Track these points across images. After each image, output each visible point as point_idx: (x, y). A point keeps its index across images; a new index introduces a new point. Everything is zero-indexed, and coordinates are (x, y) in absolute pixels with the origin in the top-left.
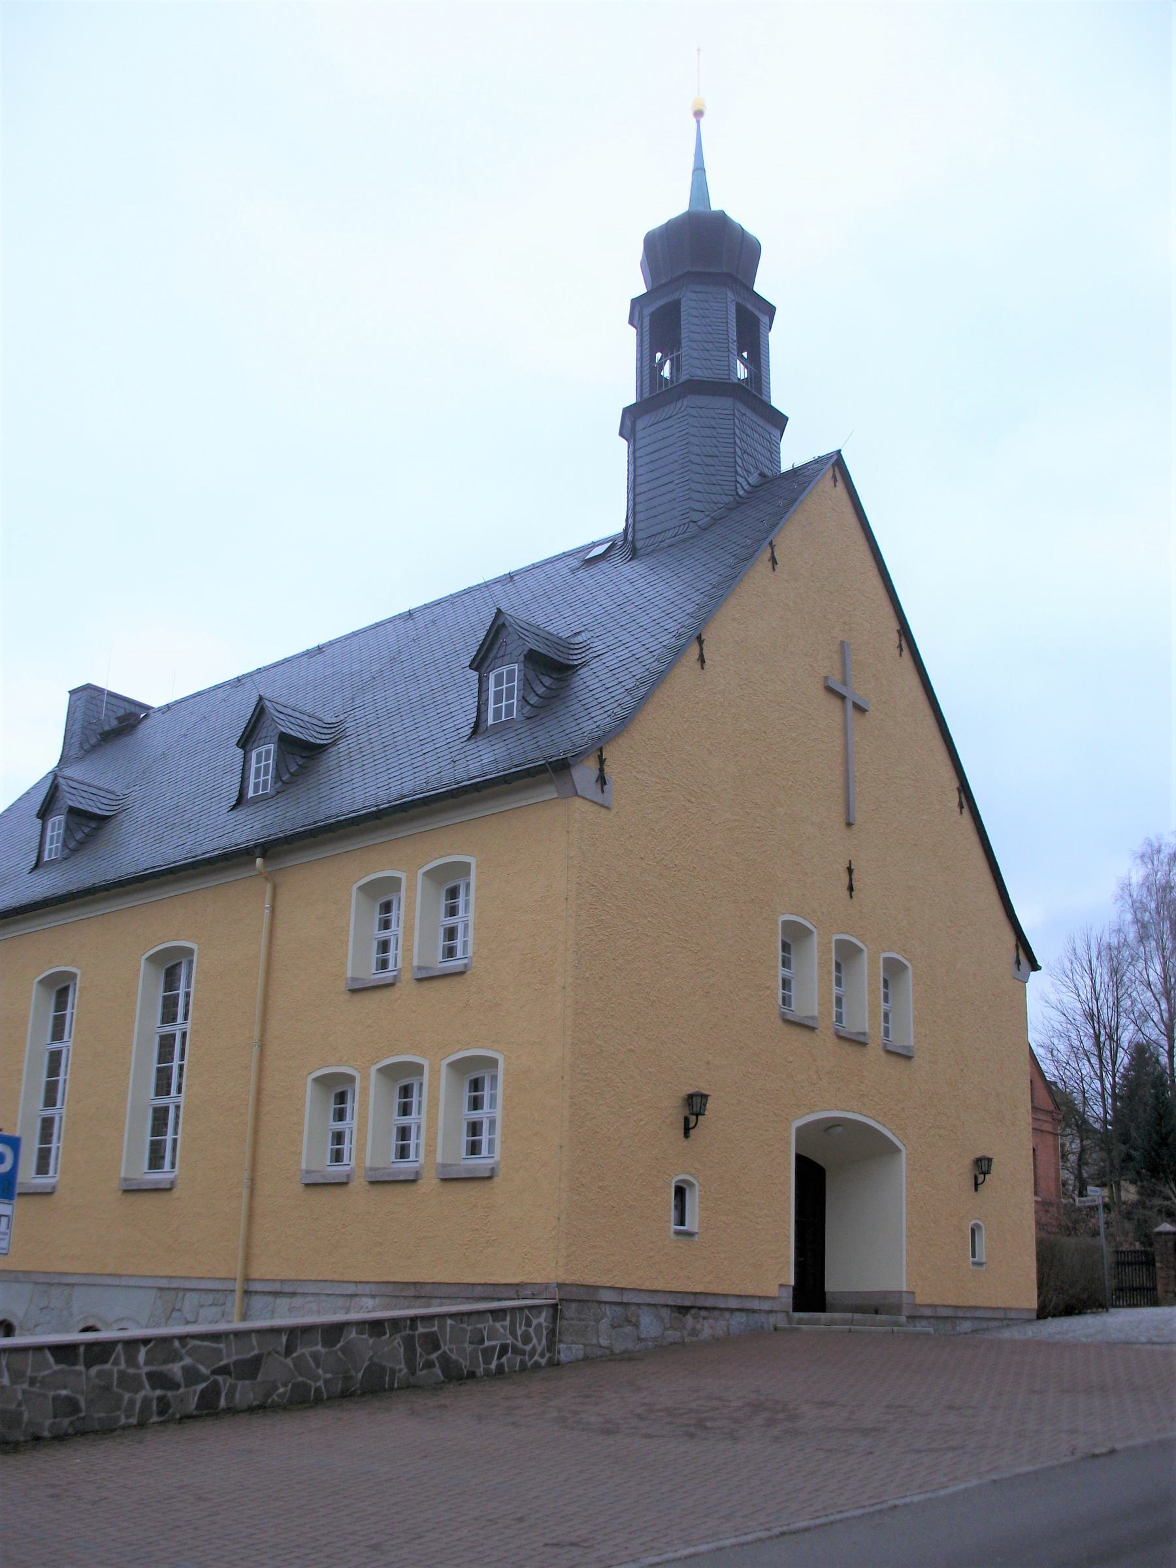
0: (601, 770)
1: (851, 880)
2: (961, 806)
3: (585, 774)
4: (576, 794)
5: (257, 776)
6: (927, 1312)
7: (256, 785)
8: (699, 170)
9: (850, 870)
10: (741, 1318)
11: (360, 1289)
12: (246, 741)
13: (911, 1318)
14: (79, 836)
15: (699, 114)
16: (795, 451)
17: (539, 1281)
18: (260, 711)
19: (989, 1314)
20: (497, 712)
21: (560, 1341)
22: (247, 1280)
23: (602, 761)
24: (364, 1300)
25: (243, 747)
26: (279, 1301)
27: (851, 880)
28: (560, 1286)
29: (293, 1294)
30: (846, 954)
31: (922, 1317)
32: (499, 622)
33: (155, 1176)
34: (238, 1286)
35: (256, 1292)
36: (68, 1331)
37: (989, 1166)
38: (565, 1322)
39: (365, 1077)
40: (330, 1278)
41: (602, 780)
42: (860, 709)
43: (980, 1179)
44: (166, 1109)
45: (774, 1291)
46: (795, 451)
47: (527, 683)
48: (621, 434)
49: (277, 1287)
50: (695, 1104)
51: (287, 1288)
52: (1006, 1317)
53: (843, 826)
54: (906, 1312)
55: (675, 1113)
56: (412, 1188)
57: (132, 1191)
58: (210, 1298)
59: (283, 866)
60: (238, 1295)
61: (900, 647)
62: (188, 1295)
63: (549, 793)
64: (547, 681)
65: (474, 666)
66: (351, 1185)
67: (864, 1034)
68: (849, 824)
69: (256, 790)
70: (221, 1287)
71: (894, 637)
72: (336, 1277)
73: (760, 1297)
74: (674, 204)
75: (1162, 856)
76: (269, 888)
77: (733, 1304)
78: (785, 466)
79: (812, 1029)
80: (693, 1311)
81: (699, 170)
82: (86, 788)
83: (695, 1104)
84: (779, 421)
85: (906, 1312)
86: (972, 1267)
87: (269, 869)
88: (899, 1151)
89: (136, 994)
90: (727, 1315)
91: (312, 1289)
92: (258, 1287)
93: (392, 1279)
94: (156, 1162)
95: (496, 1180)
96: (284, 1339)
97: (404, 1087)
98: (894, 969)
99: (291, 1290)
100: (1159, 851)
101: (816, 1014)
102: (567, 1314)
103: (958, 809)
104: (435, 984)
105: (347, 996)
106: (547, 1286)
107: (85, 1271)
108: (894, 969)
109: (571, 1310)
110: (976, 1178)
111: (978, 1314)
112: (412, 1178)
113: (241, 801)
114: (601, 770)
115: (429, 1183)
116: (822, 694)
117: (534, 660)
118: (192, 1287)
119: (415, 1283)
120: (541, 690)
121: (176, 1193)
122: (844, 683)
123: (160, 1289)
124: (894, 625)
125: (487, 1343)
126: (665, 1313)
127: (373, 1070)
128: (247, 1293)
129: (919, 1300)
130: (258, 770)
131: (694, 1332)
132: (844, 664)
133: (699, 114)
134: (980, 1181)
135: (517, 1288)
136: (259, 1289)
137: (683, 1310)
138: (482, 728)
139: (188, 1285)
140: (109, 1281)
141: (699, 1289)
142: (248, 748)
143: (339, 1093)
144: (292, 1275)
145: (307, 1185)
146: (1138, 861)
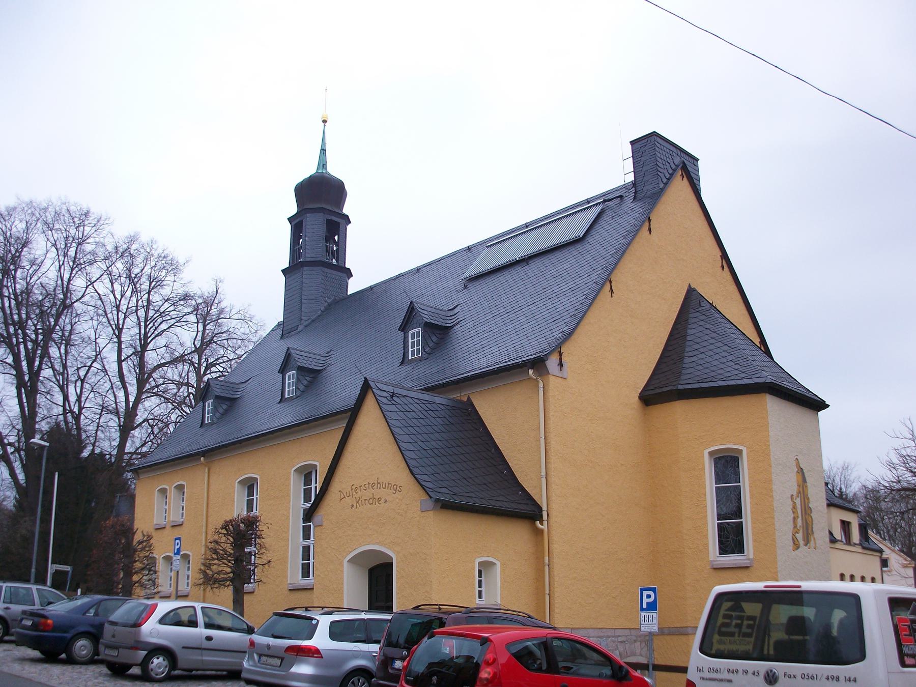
0: (561, 359)
5: (413, 347)
7: (413, 352)
8: (323, 150)
12: (283, 370)
14: (221, 411)
15: (325, 121)
18: (411, 309)
23: (561, 354)
36: (828, 579)
41: (561, 365)
44: (309, 547)
47: (298, 380)
48: (654, 134)
64: (308, 379)
69: (413, 355)
74: (309, 169)
81: (323, 150)
82: (312, 356)
84: (349, 273)
94: (306, 572)
113: (282, 399)
114: (561, 359)
117: (301, 370)
120: (431, 344)
130: (413, 343)
133: (325, 121)
138: (406, 361)
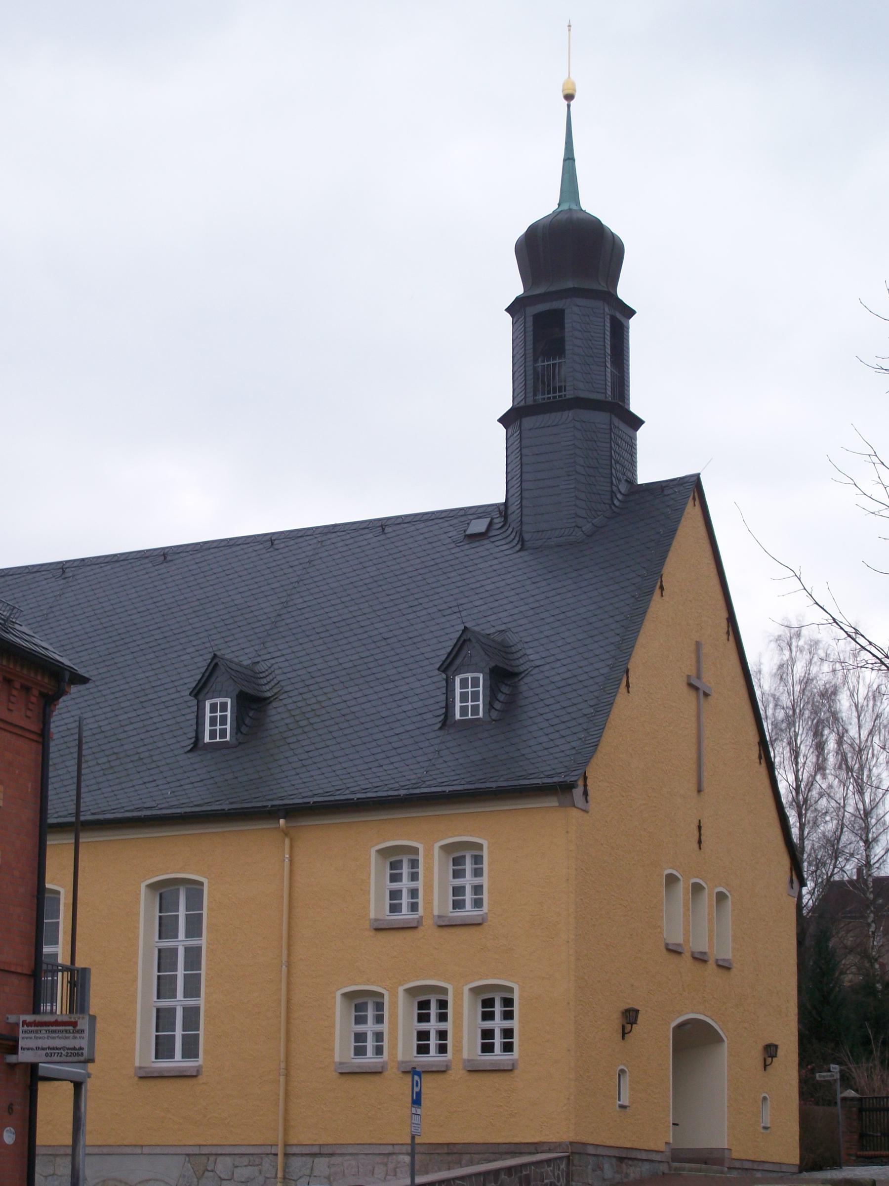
1: (700, 835)
2: (760, 757)
3: (578, 792)
4: (574, 806)
6: (737, 1164)
9: (700, 828)
10: (646, 1167)
11: (397, 1149)
13: (729, 1168)
16: (650, 469)
17: (554, 1140)
19: (770, 1167)
20: (464, 710)
21: (572, 1180)
22: (286, 1145)
24: (401, 1157)
25: (196, 696)
26: (317, 1160)
27: (700, 835)
28: (571, 1143)
29: (332, 1155)
30: (697, 889)
31: (735, 1168)
32: (464, 637)
33: (164, 1064)
34: (280, 1151)
35: (294, 1154)
37: (636, 1017)
38: (574, 1168)
39: (394, 995)
40: (369, 1142)
42: (706, 695)
43: (769, 1060)
45: (662, 1147)
46: (650, 469)
49: (316, 1150)
50: (630, 1016)
51: (325, 1150)
52: (776, 1171)
53: (696, 793)
54: (726, 1165)
55: (616, 1020)
56: (441, 1077)
57: (147, 1077)
58: (245, 1160)
59: (299, 824)
60: (280, 1157)
61: (728, 633)
62: (220, 1159)
63: (553, 802)
65: (442, 668)
66: (385, 1074)
67: (705, 953)
68: (699, 791)
70: (260, 1152)
71: (724, 624)
72: (374, 1141)
73: (646, 1150)
75: (801, 643)
76: (287, 841)
77: (644, 1156)
78: (643, 477)
79: (680, 953)
80: (626, 1161)
83: (630, 1016)
85: (726, 1165)
86: (762, 1131)
87: (290, 825)
88: (723, 1040)
89: (138, 914)
90: (640, 1164)
91: (351, 1150)
92: (295, 1150)
93: (427, 1142)
95: (516, 1072)
96: (563, 1166)
97: (428, 1004)
98: (721, 897)
99: (330, 1151)
100: (798, 635)
101: (682, 942)
102: (576, 1162)
103: (758, 761)
104: (453, 930)
105: (372, 933)
106: (560, 1144)
107: (99, 1143)
108: (721, 897)
109: (576, 1159)
110: (765, 1060)
111: (766, 1167)
112: (443, 1069)
115: (457, 1073)
116: (685, 689)
118: (236, 1152)
119: (448, 1144)
121: (202, 1079)
122: (699, 677)
123: (188, 1155)
124: (724, 614)
125: (546, 1181)
126: (614, 1160)
127: (401, 989)
128: (286, 1155)
129: (735, 1155)
131: (627, 1175)
132: (698, 661)
134: (768, 1063)
135: (536, 1147)
136: (297, 1152)
137: (621, 1159)
139: (220, 1151)
140: (128, 1150)
141: (628, 1145)
142: (201, 697)
143: (362, 1003)
144: (331, 1141)
145: (341, 1073)
146: (773, 645)
